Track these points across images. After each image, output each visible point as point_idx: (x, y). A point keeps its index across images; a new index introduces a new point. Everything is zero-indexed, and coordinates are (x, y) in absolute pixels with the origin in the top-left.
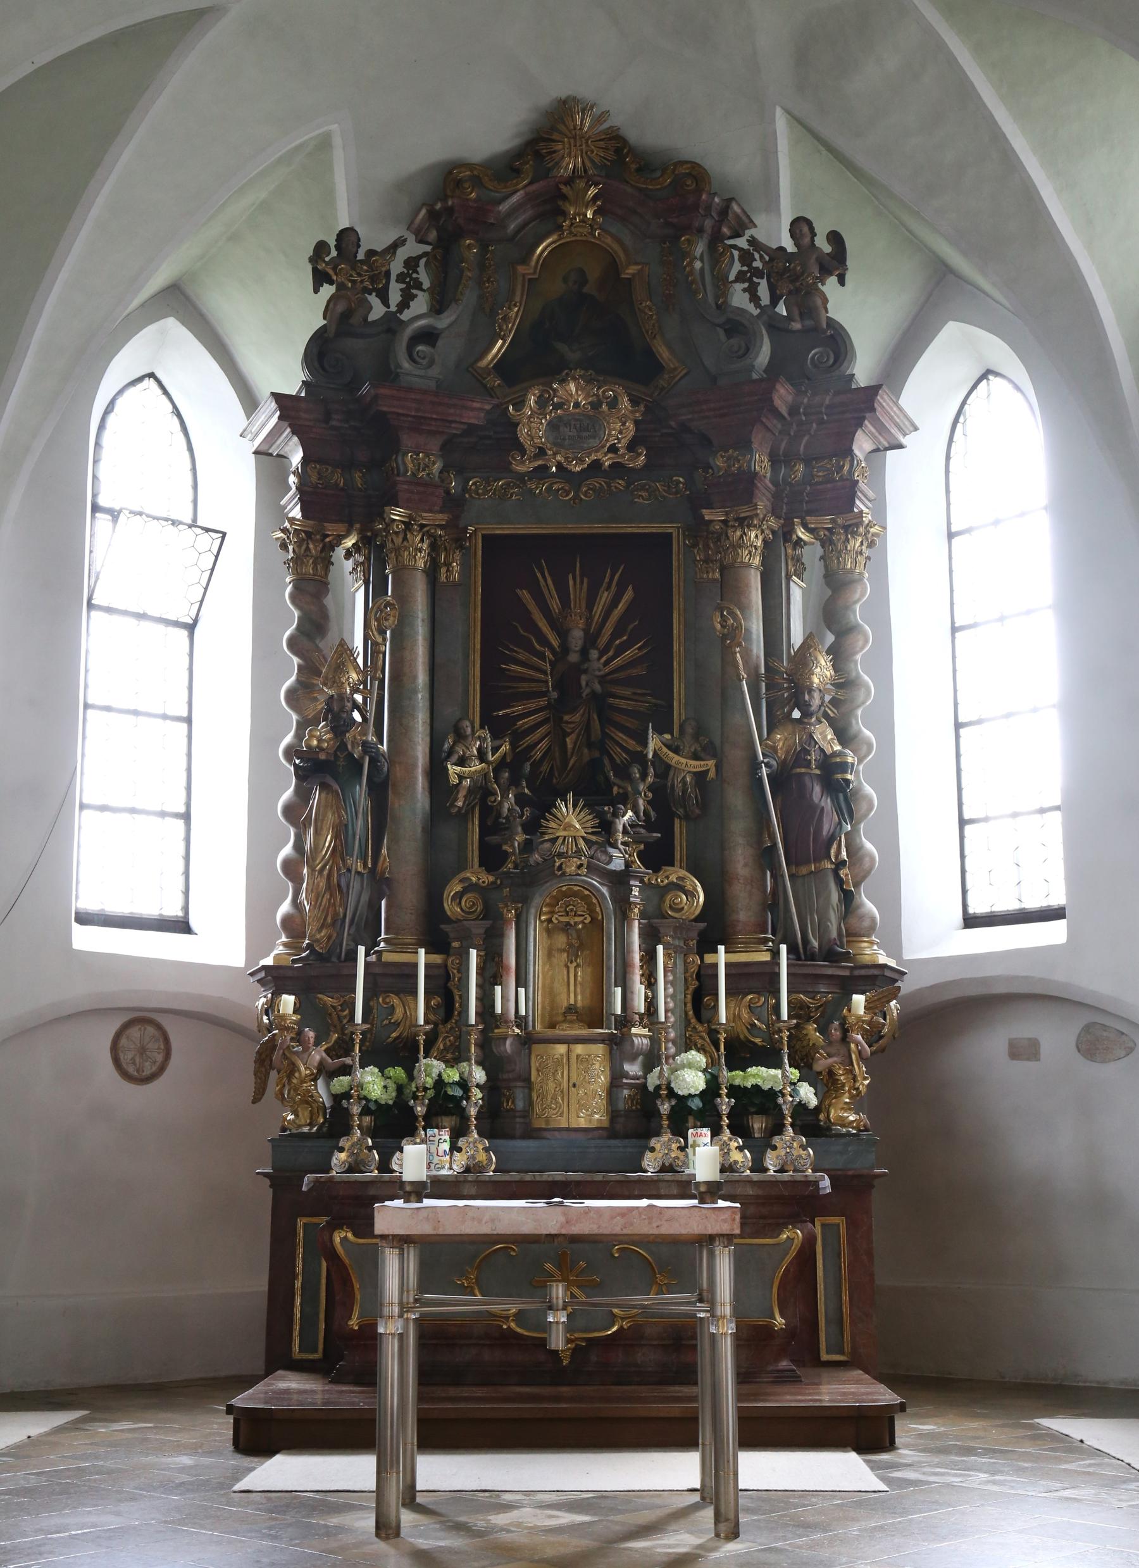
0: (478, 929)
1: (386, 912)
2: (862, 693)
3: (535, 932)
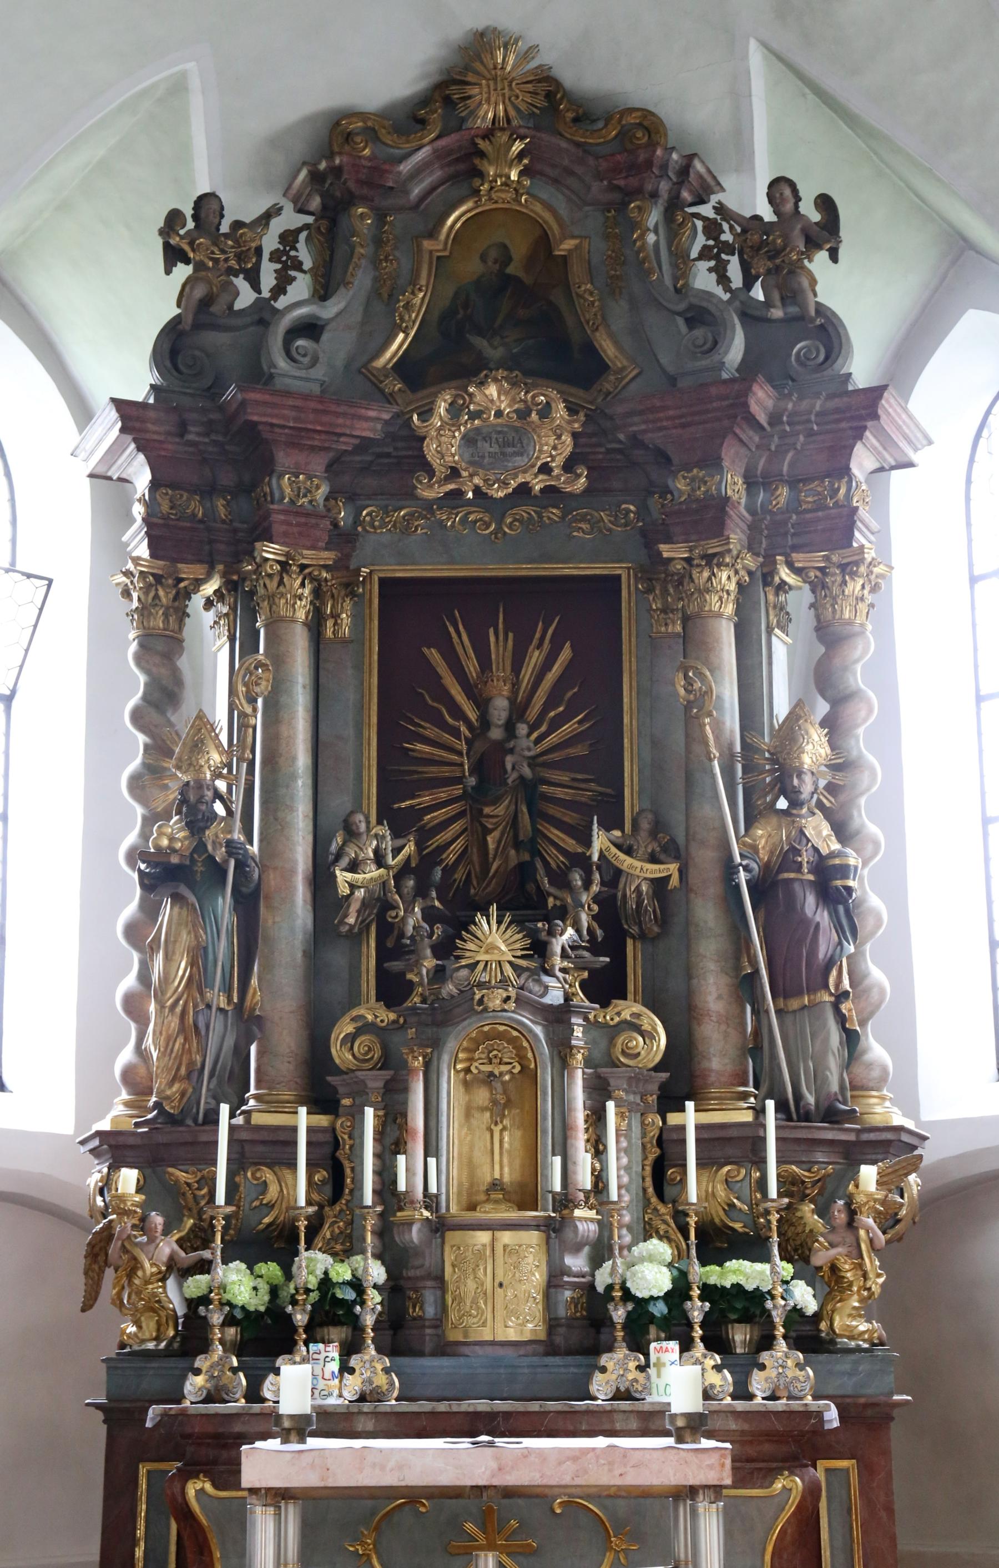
0: (376, 1081)
2: (865, 778)
3: (449, 1083)
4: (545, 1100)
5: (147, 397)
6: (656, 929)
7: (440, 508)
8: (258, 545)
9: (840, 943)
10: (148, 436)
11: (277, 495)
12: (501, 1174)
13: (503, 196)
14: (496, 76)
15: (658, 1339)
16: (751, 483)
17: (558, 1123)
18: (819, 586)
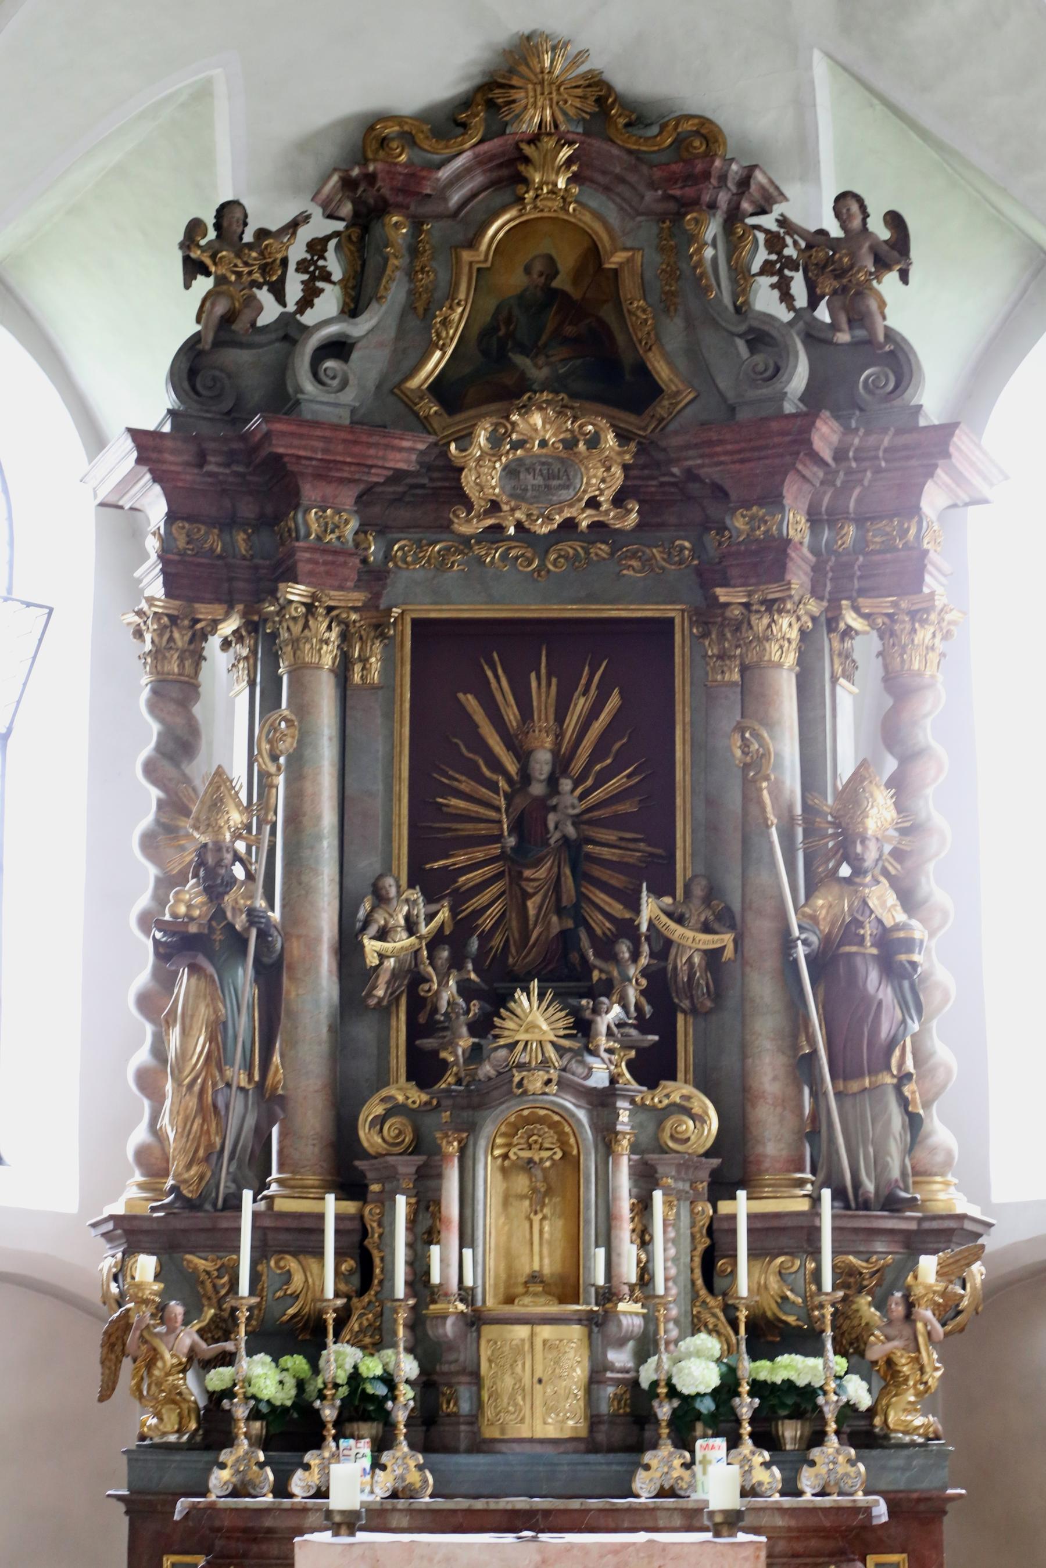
0: (407, 1166)
1: (280, 1142)
4: (587, 1188)
5: (162, 423)
6: (709, 1004)
7: (478, 542)
8: (282, 586)
9: (904, 1021)
10: (165, 467)
11: (302, 532)
12: (541, 1266)
13: (549, 204)
14: (542, 81)
15: (705, 1436)
16: (814, 519)
17: (602, 1214)
18: (887, 634)
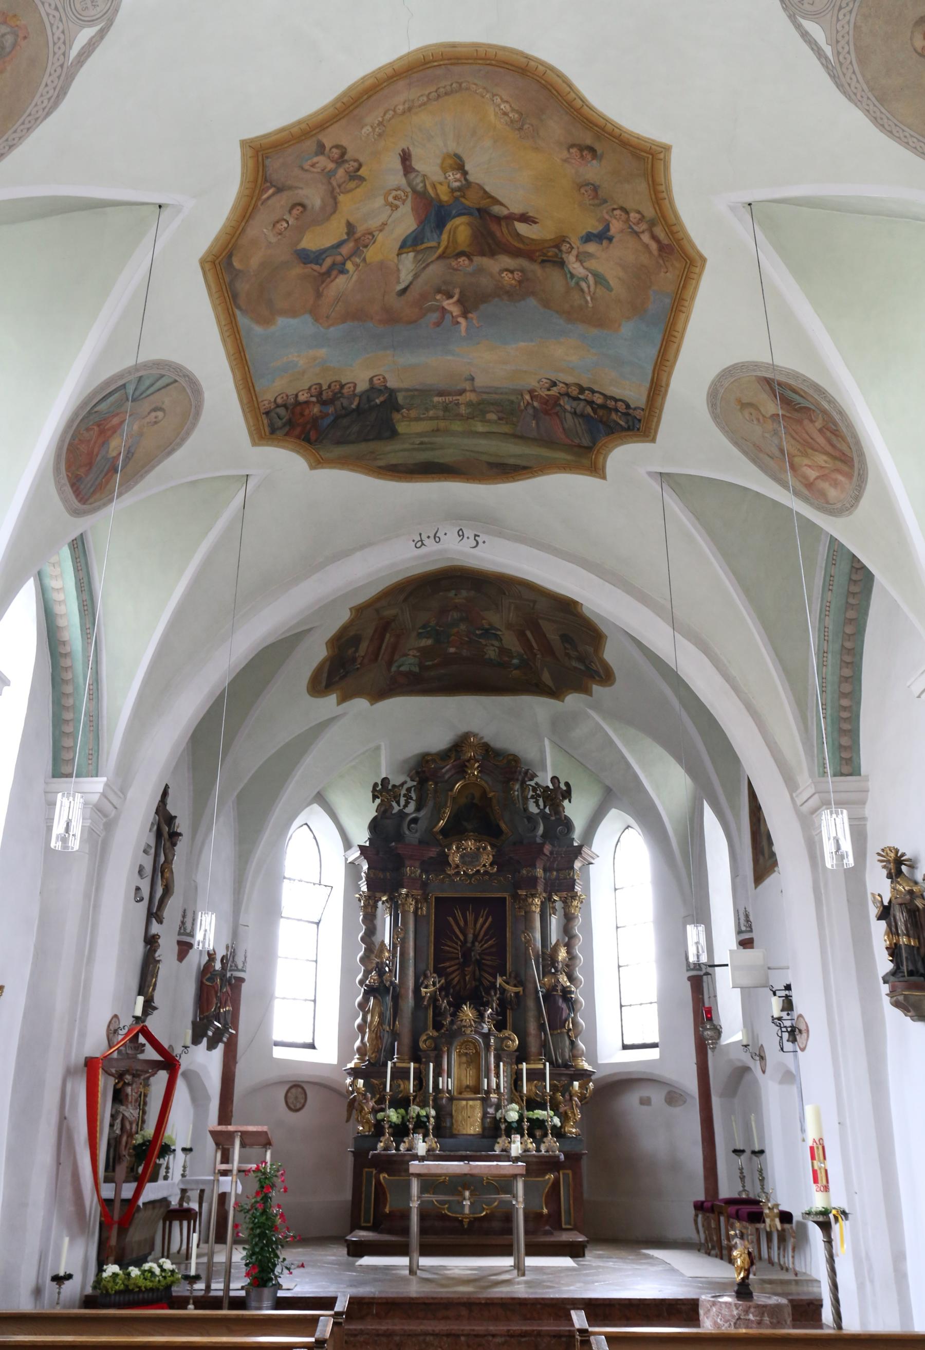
0: (433, 1054)
2: (578, 961)
3: (454, 1056)
14: (471, 745)
16: (545, 870)
